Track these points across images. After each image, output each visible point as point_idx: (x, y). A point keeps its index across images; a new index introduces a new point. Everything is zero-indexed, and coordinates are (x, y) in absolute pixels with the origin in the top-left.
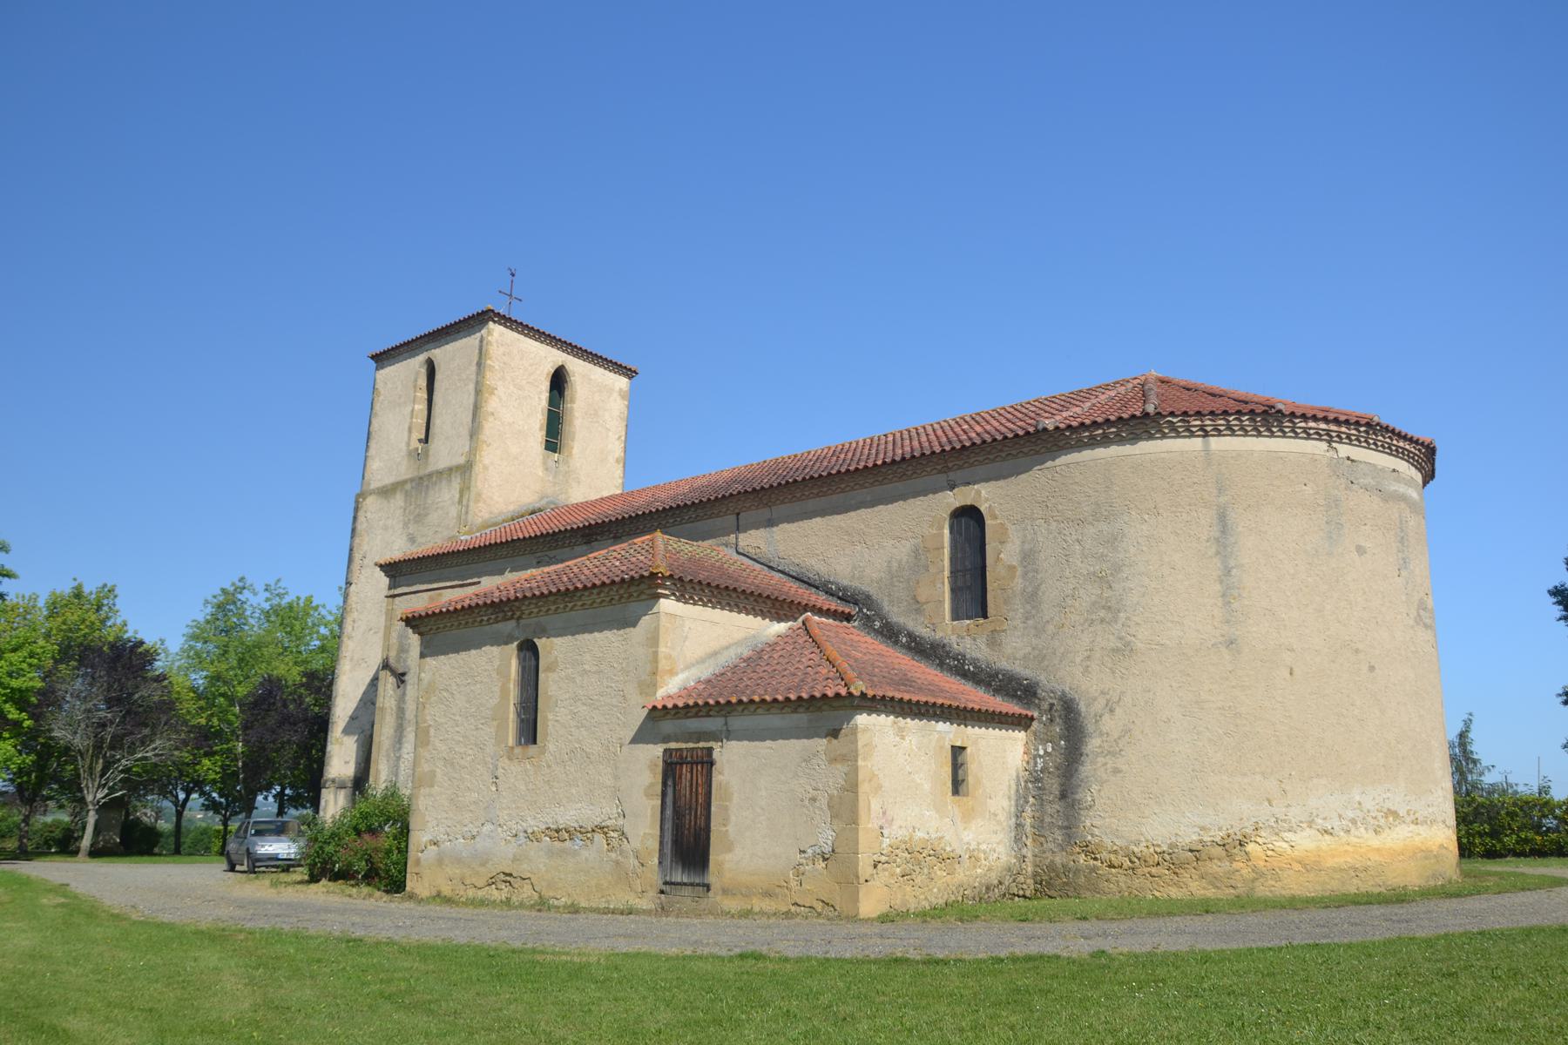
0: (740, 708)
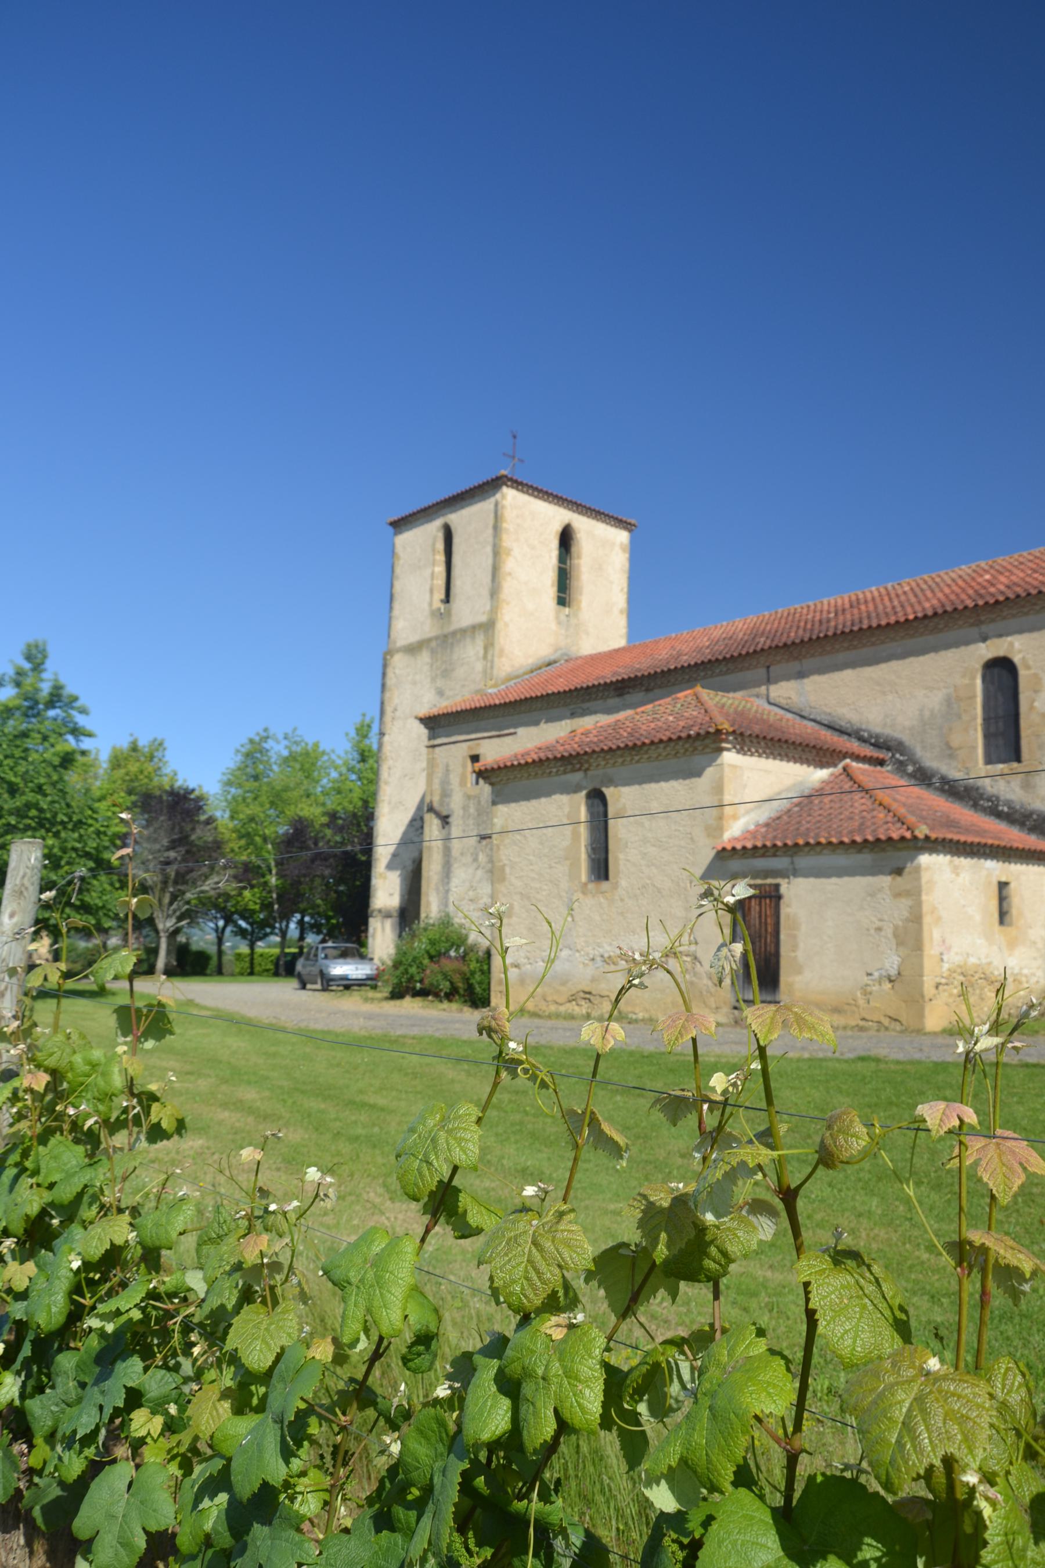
0: (807, 849)
